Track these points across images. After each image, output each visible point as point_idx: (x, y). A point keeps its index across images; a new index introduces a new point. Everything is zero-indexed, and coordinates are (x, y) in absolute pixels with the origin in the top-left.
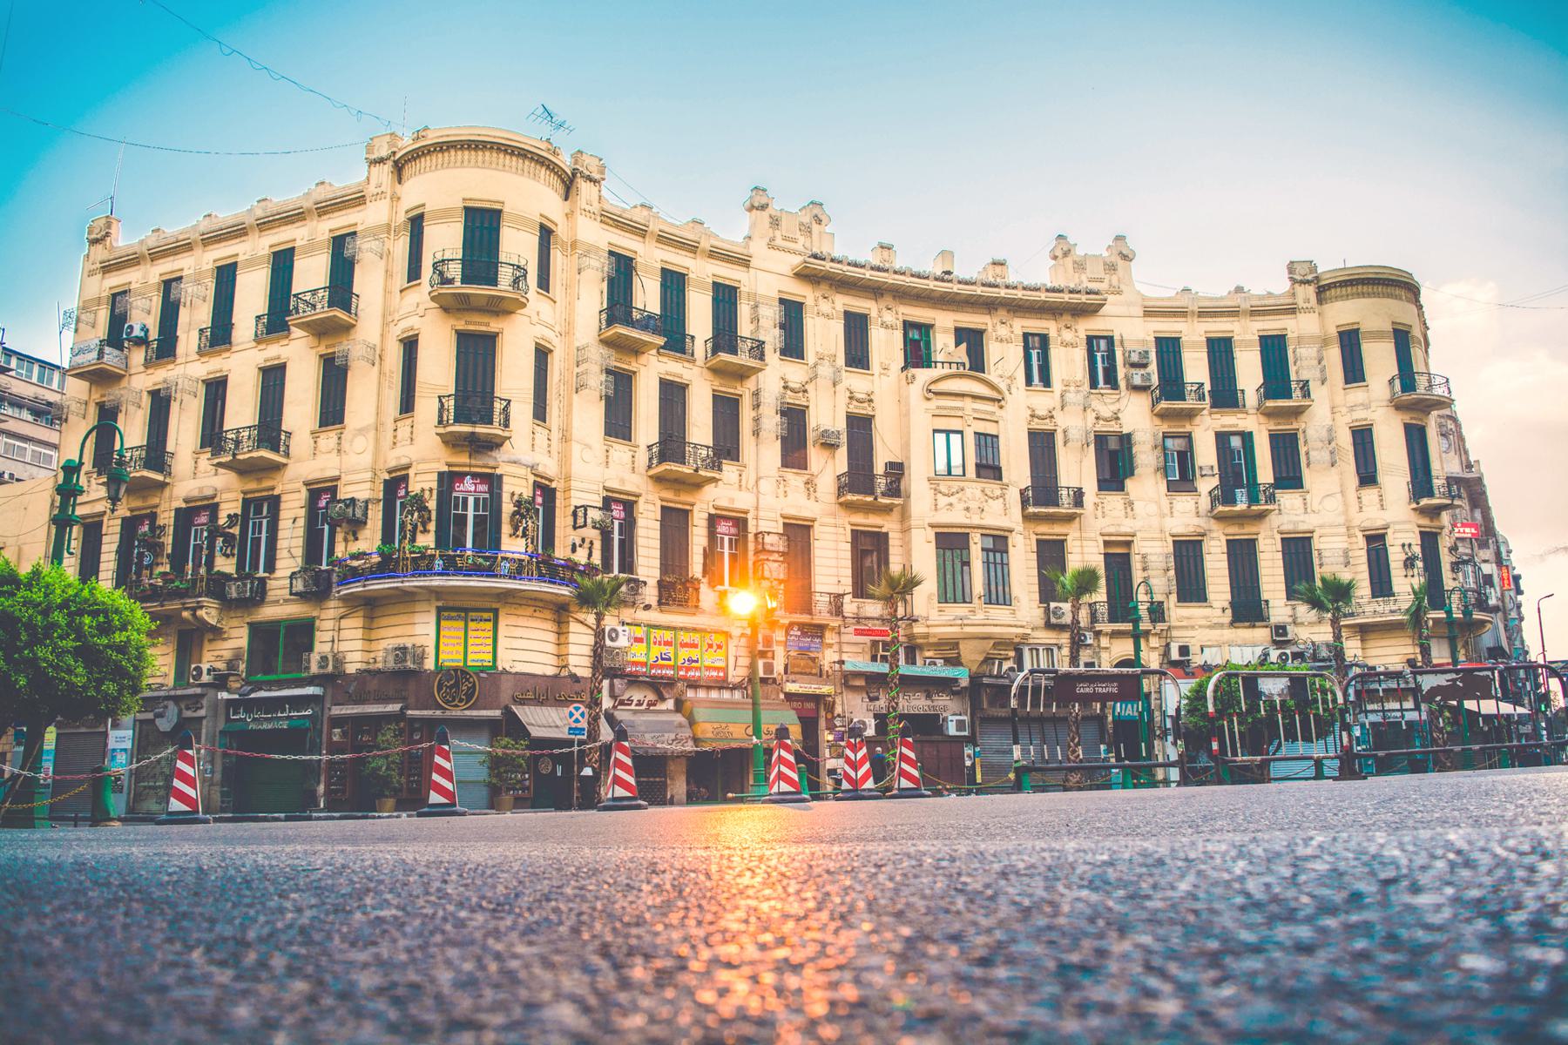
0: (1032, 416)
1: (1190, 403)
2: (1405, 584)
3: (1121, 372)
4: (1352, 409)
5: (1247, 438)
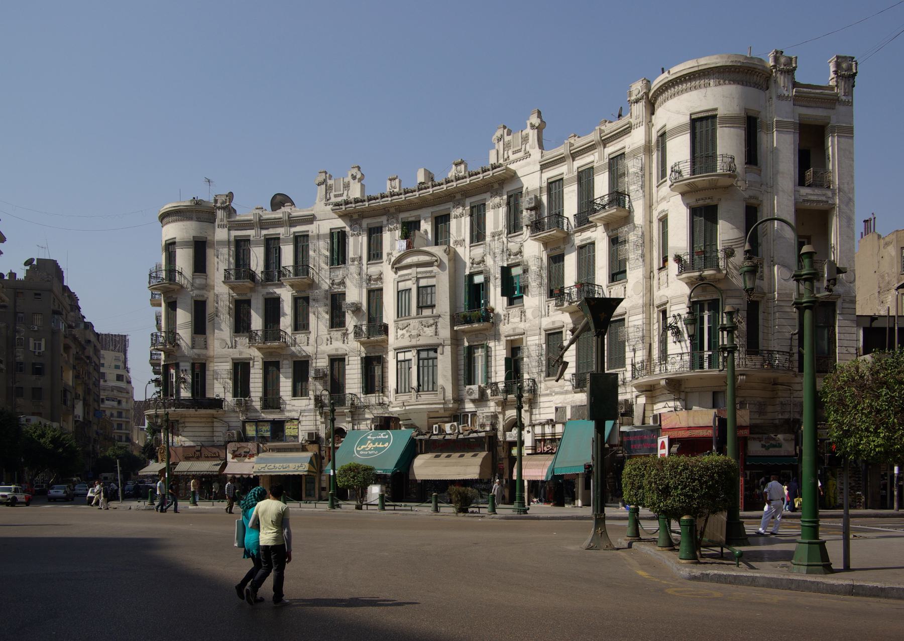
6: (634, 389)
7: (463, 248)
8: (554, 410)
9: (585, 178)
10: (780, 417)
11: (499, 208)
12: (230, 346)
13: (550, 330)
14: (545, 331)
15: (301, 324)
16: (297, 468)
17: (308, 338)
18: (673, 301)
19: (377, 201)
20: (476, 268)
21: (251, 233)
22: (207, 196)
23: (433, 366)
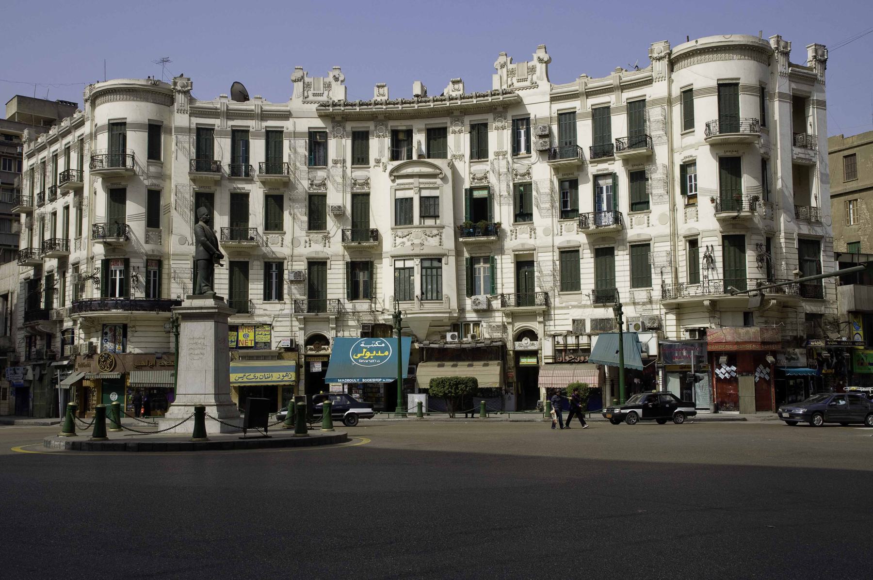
0: (474, 179)
6: (662, 307)
7: (462, 163)
8: (571, 322)
9: (601, 117)
10: (791, 334)
11: (503, 129)
12: (191, 242)
13: (564, 248)
14: (559, 248)
15: (273, 223)
16: (282, 378)
17: (282, 238)
18: (705, 234)
19: (369, 107)
20: (477, 183)
21: (216, 122)
22: (167, 77)
23: (437, 275)
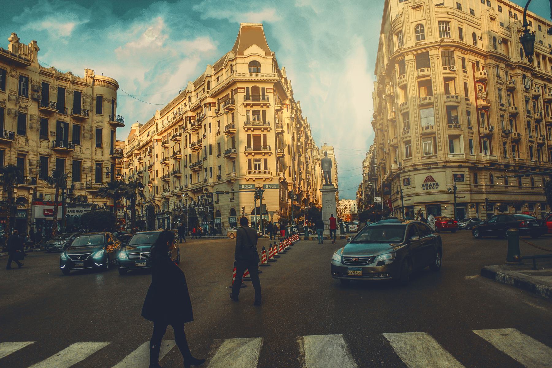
1: (50, 108)
2: (106, 180)
3: (30, 92)
4: (97, 122)
5: (66, 125)
